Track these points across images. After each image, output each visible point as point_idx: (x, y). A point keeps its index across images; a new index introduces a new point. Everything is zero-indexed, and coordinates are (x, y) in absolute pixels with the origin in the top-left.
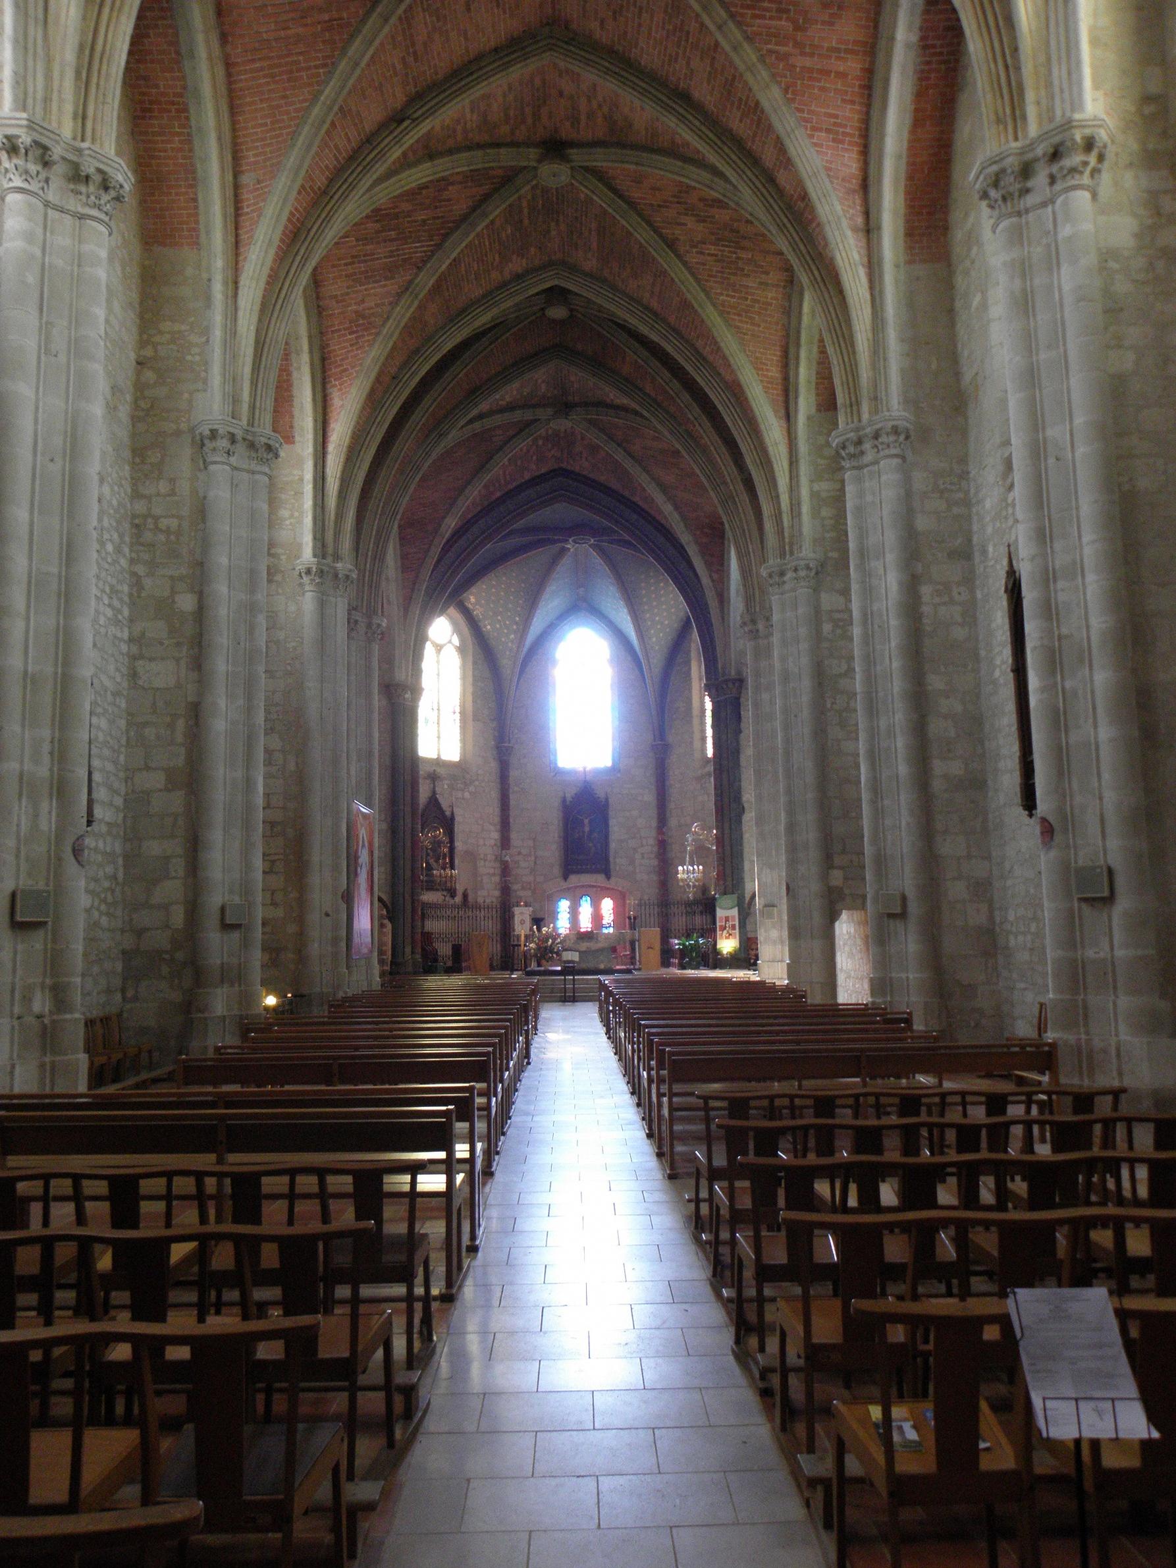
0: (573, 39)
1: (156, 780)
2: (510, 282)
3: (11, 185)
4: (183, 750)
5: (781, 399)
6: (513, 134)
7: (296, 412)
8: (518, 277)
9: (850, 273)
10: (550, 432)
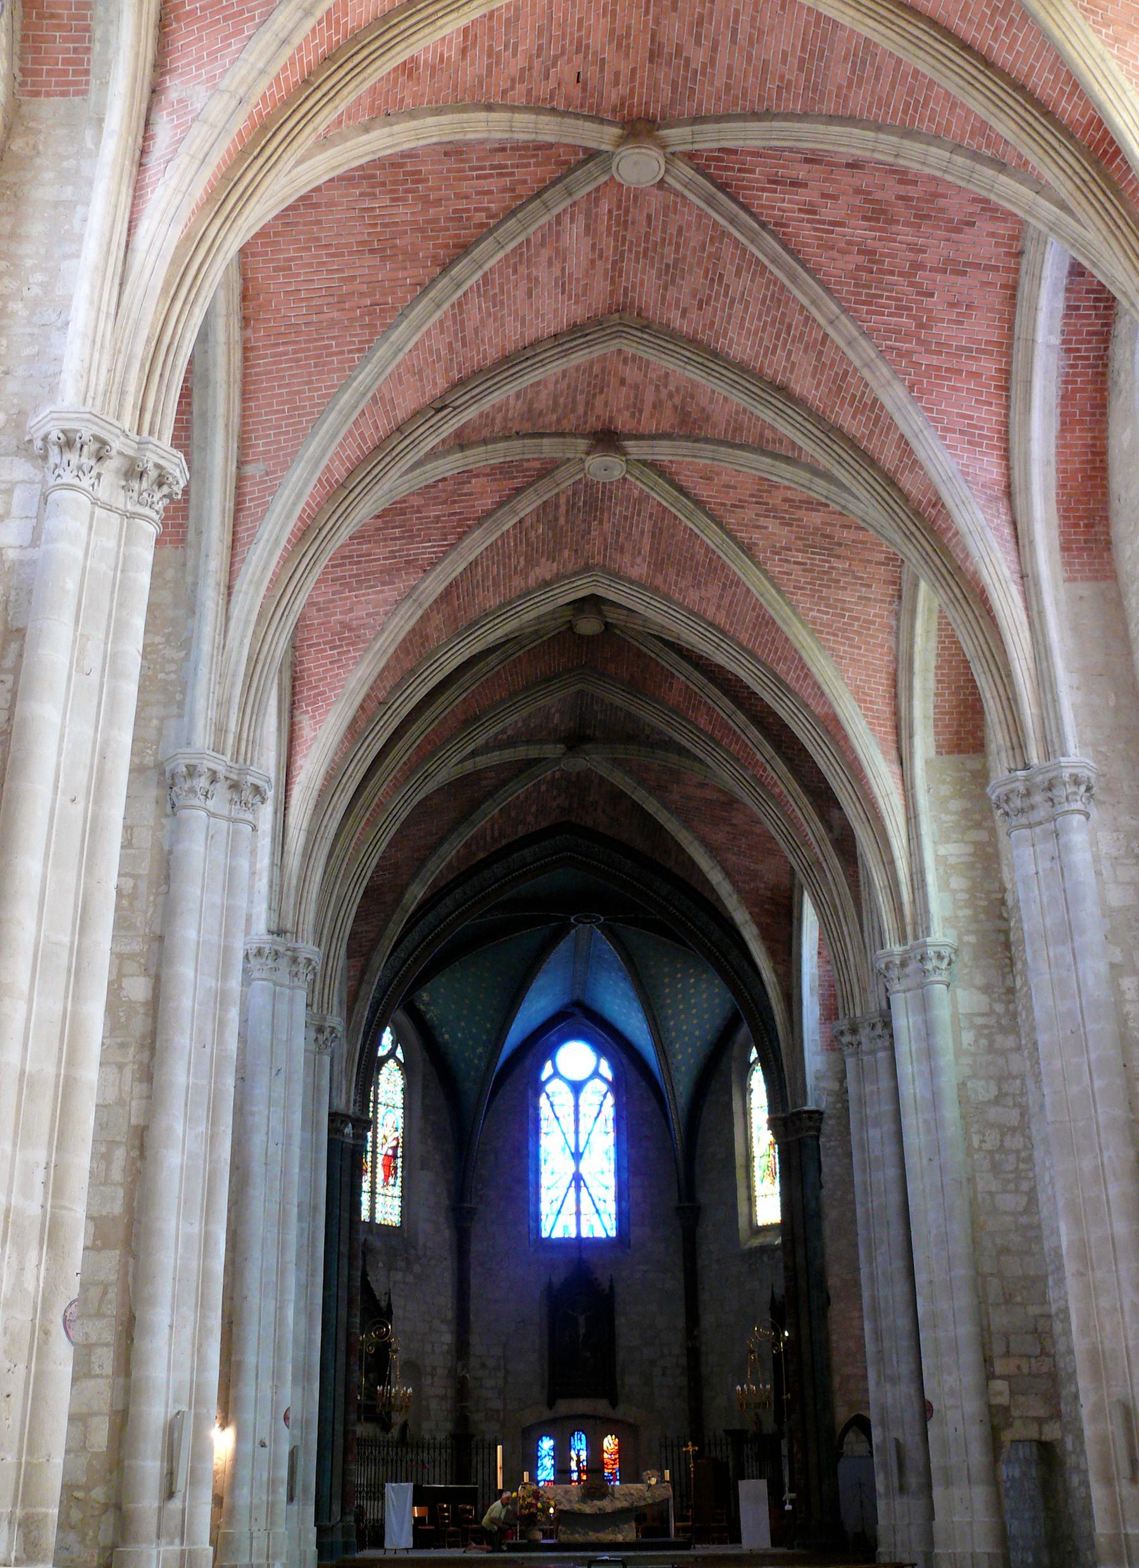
0: (646, 327)
3: (59, 481)
4: (120, 1192)
5: (891, 737)
6: (558, 421)
8: (546, 584)
10: (558, 775)
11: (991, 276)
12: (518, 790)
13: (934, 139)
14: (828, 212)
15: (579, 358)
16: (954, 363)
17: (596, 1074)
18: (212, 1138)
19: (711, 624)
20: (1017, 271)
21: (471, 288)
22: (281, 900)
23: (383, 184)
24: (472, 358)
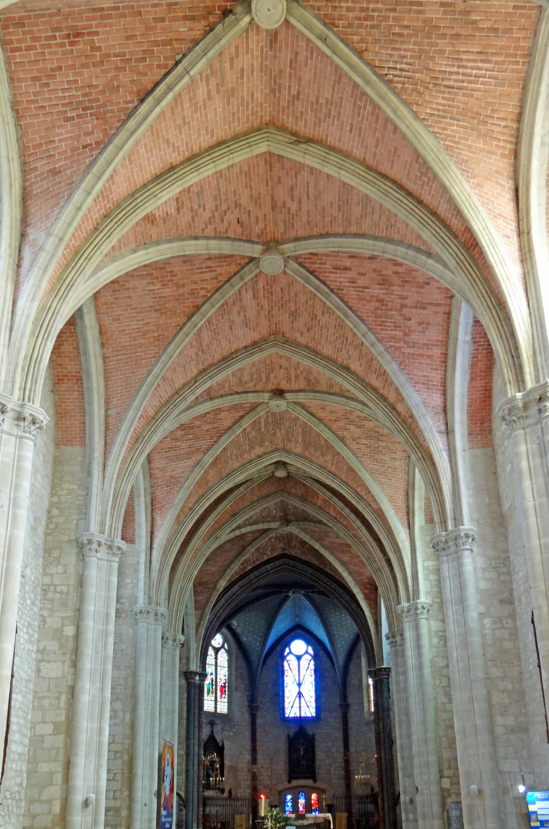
1: (48, 729)
2: (254, 459)
4: (64, 712)
5: (405, 517)
6: (255, 386)
7: (136, 527)
9: (438, 455)
10: (278, 535)
11: (438, 309)
12: (262, 542)
13: (400, 243)
14: (362, 282)
15: (256, 357)
16: (420, 352)
17: (307, 652)
18: (102, 689)
19: (330, 472)
20: (450, 305)
21: (203, 325)
22: (149, 590)
23: (157, 278)
24: (208, 359)
